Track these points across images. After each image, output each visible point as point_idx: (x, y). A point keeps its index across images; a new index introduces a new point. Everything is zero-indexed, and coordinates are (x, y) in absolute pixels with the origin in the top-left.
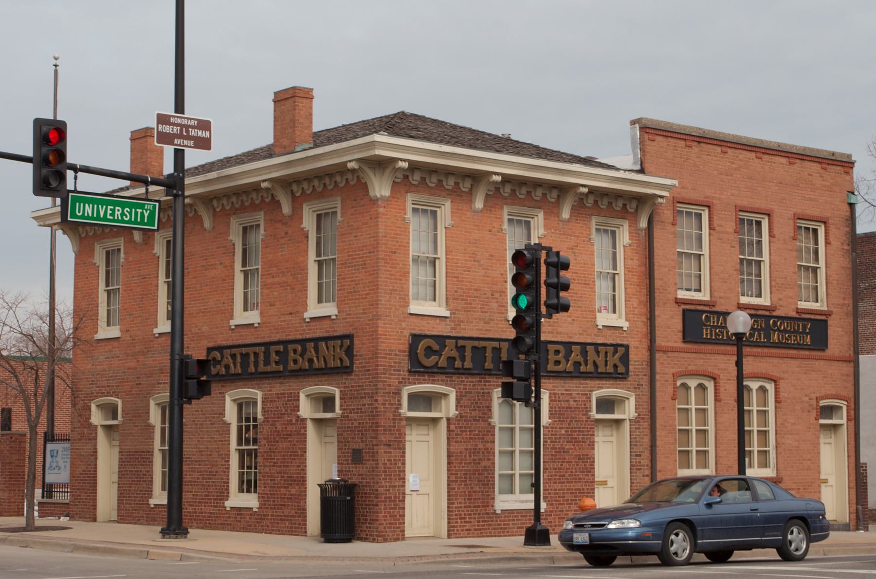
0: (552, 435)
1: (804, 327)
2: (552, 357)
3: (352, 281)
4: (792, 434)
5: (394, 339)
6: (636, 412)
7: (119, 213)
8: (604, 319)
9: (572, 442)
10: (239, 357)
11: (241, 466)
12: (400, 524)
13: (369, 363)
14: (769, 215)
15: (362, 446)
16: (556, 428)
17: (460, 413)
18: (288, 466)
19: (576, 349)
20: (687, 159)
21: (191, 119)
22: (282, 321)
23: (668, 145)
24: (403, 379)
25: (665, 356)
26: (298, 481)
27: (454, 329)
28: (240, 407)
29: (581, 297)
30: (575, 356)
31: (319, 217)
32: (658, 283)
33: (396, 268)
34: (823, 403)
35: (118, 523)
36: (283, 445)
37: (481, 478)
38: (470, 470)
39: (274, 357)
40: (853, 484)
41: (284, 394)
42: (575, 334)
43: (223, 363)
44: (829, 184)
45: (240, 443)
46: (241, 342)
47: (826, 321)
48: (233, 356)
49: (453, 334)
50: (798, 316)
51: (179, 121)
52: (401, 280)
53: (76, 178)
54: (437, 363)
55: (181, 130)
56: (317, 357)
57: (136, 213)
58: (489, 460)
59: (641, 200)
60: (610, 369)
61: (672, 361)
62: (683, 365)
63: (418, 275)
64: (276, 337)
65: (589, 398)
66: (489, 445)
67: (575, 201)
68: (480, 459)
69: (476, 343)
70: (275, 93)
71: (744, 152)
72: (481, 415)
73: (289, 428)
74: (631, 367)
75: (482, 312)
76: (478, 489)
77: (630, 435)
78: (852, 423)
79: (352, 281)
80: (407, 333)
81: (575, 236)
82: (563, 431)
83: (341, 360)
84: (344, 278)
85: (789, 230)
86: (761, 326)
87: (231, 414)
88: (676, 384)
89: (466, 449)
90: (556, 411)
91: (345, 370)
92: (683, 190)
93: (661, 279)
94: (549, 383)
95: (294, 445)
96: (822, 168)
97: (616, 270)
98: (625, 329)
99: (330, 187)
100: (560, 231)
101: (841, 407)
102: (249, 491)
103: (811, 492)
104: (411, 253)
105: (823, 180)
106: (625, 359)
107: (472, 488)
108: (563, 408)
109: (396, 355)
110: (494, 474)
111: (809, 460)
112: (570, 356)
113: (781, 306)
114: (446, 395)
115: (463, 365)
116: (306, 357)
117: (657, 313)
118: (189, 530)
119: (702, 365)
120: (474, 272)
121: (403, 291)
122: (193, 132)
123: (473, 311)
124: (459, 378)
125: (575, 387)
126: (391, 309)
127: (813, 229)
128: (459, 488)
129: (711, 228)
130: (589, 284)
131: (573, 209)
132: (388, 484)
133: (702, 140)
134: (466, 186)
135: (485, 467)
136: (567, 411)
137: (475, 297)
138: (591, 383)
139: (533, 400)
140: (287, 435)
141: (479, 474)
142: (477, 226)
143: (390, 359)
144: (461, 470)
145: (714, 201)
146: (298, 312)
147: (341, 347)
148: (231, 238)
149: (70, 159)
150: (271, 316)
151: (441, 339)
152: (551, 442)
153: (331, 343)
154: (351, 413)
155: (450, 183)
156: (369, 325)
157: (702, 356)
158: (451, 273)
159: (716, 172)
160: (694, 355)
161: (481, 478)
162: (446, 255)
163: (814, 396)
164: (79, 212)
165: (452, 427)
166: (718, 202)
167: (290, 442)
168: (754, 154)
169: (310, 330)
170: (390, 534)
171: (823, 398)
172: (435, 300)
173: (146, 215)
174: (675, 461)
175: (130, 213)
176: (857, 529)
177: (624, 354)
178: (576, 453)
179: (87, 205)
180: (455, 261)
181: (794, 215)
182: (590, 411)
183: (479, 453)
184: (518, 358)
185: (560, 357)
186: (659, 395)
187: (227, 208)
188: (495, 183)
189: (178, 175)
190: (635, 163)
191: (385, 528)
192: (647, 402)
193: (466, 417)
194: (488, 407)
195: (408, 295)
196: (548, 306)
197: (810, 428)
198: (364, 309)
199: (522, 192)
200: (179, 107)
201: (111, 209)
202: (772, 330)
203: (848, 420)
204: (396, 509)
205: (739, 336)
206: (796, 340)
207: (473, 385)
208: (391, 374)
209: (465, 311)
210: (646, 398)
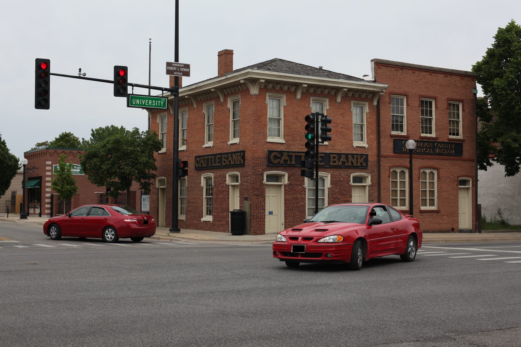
0: (332, 192)
1: (451, 146)
2: (332, 159)
3: (244, 129)
4: (445, 192)
5: (260, 152)
6: (371, 182)
7: (151, 103)
8: (356, 144)
9: (341, 195)
10: (205, 160)
11: (207, 205)
12: (263, 228)
13: (250, 162)
14: (435, 99)
15: (248, 196)
16: (334, 189)
17: (290, 183)
18: (222, 204)
19: (343, 156)
20: (396, 76)
21: (181, 64)
22: (221, 145)
23: (387, 70)
24: (264, 169)
25: (385, 159)
26: (226, 210)
27: (287, 148)
28: (207, 180)
29: (346, 134)
30: (343, 159)
31: (234, 103)
32: (382, 128)
33: (261, 123)
34: (460, 179)
35: (166, 227)
36: (221, 196)
37: (299, 209)
38: (294, 206)
39: (218, 160)
40: (474, 213)
41: (221, 175)
42: (343, 150)
43: (200, 163)
44: (464, 85)
45: (207, 195)
46: (207, 154)
47: (462, 144)
48: (204, 160)
49: (287, 150)
50: (448, 142)
51: (176, 65)
52: (263, 128)
53: (133, 89)
54: (279, 162)
55: (177, 69)
56: (232, 160)
57: (158, 103)
58: (303, 202)
59: (374, 94)
60: (359, 164)
61: (389, 161)
62: (394, 162)
63: (271, 126)
64: (219, 152)
65: (350, 177)
66: (303, 196)
67: (343, 94)
68: (299, 202)
69: (297, 154)
70: (219, 52)
71: (423, 72)
72: (299, 184)
73: (223, 189)
74: (369, 164)
75: (300, 141)
76: (298, 214)
77: (369, 192)
78: (474, 187)
79: (244, 129)
80: (266, 150)
81: (343, 109)
82: (337, 190)
83: (240, 161)
84: (242, 128)
85: (445, 105)
86: (431, 146)
87: (203, 183)
88: (420, 172)
89: (293, 198)
90: (334, 182)
91: (242, 165)
92: (394, 89)
93: (383, 127)
94: (331, 170)
95: (225, 196)
96: (461, 79)
97: (363, 123)
98: (366, 148)
99: (237, 91)
100: (336, 107)
101: (469, 181)
102: (210, 215)
103: (454, 216)
104: (268, 117)
105: (461, 84)
106: (366, 160)
107: (295, 214)
108: (337, 180)
109: (261, 159)
110: (305, 208)
111: (453, 203)
112: (340, 159)
113: (440, 137)
114: (284, 176)
115: (291, 163)
116: (228, 160)
117: (381, 141)
118: (181, 229)
119: (402, 163)
120: (296, 124)
121: (264, 133)
122: (182, 69)
123: (296, 141)
124: (289, 168)
125: (343, 173)
126: (259, 140)
127: (429, 102)
128: (289, 214)
129: (408, 105)
130: (349, 129)
131: (342, 97)
132: (257, 211)
133: (403, 68)
134: (293, 89)
135: (301, 205)
136: (339, 182)
137: (297, 135)
138: (350, 170)
139: (315, 177)
140: (222, 192)
141: (299, 208)
142: (298, 105)
143: (258, 160)
144: (291, 206)
145: (409, 93)
146: (226, 142)
147: (240, 156)
148: (203, 112)
149: (129, 81)
150: (217, 143)
151: (281, 152)
152: (332, 195)
153: (237, 154)
154: (244, 183)
155: (286, 88)
156: (250, 147)
157: (403, 159)
158: (286, 125)
159: (410, 81)
160: (399, 159)
161: (299, 209)
162: (284, 117)
163: (456, 176)
164: (134, 103)
165: (287, 188)
166: (411, 94)
167: (223, 194)
168: (428, 73)
169: (230, 149)
170: (259, 232)
171: (460, 176)
172: (279, 136)
173: (162, 103)
174: (390, 203)
175: (155, 103)
176: (475, 232)
177: (365, 158)
178: (343, 199)
179: (137, 100)
180: (288, 120)
181: (447, 99)
182: (350, 182)
183: (298, 199)
184: (308, 160)
185: (336, 160)
186: (382, 176)
187: (202, 99)
188: (305, 87)
189: (176, 87)
190: (372, 78)
191: (256, 229)
192: (377, 178)
193: (293, 184)
194: (303, 180)
195: (267, 134)
196: (322, 138)
197: (454, 189)
198: (248, 140)
199: (319, 91)
200: (177, 58)
201: (147, 101)
202: (436, 148)
203: (473, 186)
204: (261, 221)
205: (411, 150)
206: (448, 151)
207: (296, 171)
208: (259, 167)
209: (292, 141)
210: (376, 177)
